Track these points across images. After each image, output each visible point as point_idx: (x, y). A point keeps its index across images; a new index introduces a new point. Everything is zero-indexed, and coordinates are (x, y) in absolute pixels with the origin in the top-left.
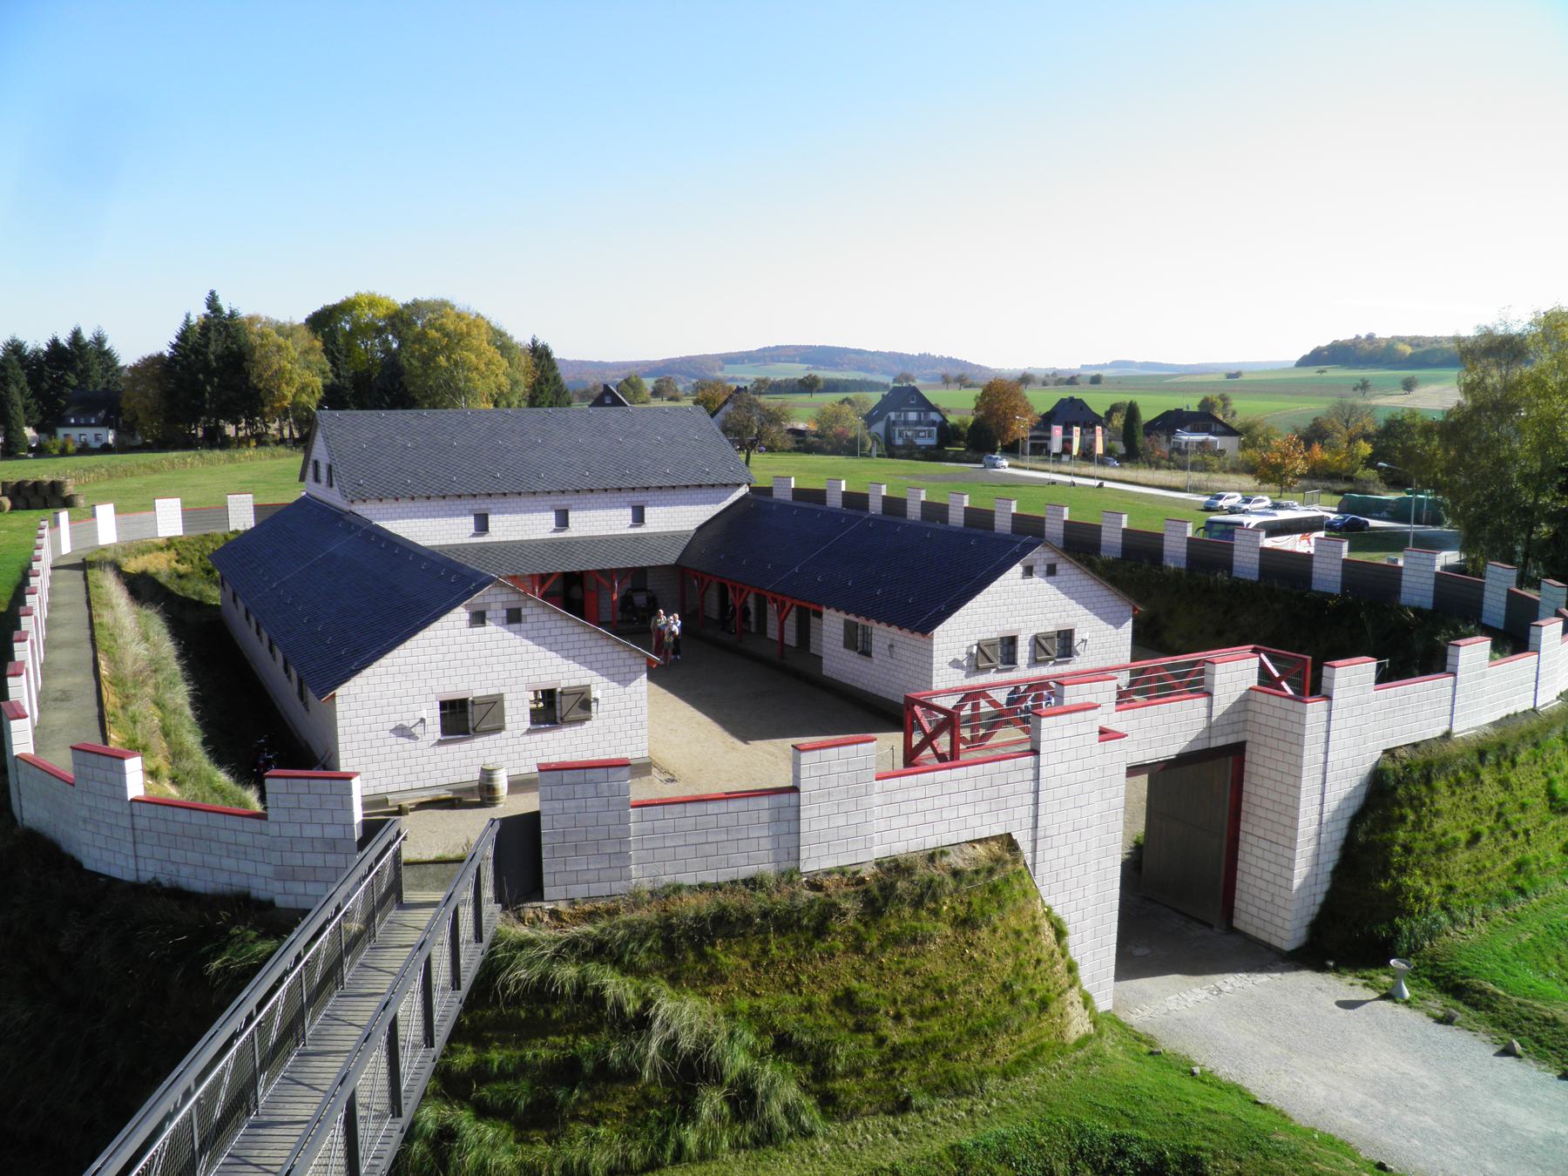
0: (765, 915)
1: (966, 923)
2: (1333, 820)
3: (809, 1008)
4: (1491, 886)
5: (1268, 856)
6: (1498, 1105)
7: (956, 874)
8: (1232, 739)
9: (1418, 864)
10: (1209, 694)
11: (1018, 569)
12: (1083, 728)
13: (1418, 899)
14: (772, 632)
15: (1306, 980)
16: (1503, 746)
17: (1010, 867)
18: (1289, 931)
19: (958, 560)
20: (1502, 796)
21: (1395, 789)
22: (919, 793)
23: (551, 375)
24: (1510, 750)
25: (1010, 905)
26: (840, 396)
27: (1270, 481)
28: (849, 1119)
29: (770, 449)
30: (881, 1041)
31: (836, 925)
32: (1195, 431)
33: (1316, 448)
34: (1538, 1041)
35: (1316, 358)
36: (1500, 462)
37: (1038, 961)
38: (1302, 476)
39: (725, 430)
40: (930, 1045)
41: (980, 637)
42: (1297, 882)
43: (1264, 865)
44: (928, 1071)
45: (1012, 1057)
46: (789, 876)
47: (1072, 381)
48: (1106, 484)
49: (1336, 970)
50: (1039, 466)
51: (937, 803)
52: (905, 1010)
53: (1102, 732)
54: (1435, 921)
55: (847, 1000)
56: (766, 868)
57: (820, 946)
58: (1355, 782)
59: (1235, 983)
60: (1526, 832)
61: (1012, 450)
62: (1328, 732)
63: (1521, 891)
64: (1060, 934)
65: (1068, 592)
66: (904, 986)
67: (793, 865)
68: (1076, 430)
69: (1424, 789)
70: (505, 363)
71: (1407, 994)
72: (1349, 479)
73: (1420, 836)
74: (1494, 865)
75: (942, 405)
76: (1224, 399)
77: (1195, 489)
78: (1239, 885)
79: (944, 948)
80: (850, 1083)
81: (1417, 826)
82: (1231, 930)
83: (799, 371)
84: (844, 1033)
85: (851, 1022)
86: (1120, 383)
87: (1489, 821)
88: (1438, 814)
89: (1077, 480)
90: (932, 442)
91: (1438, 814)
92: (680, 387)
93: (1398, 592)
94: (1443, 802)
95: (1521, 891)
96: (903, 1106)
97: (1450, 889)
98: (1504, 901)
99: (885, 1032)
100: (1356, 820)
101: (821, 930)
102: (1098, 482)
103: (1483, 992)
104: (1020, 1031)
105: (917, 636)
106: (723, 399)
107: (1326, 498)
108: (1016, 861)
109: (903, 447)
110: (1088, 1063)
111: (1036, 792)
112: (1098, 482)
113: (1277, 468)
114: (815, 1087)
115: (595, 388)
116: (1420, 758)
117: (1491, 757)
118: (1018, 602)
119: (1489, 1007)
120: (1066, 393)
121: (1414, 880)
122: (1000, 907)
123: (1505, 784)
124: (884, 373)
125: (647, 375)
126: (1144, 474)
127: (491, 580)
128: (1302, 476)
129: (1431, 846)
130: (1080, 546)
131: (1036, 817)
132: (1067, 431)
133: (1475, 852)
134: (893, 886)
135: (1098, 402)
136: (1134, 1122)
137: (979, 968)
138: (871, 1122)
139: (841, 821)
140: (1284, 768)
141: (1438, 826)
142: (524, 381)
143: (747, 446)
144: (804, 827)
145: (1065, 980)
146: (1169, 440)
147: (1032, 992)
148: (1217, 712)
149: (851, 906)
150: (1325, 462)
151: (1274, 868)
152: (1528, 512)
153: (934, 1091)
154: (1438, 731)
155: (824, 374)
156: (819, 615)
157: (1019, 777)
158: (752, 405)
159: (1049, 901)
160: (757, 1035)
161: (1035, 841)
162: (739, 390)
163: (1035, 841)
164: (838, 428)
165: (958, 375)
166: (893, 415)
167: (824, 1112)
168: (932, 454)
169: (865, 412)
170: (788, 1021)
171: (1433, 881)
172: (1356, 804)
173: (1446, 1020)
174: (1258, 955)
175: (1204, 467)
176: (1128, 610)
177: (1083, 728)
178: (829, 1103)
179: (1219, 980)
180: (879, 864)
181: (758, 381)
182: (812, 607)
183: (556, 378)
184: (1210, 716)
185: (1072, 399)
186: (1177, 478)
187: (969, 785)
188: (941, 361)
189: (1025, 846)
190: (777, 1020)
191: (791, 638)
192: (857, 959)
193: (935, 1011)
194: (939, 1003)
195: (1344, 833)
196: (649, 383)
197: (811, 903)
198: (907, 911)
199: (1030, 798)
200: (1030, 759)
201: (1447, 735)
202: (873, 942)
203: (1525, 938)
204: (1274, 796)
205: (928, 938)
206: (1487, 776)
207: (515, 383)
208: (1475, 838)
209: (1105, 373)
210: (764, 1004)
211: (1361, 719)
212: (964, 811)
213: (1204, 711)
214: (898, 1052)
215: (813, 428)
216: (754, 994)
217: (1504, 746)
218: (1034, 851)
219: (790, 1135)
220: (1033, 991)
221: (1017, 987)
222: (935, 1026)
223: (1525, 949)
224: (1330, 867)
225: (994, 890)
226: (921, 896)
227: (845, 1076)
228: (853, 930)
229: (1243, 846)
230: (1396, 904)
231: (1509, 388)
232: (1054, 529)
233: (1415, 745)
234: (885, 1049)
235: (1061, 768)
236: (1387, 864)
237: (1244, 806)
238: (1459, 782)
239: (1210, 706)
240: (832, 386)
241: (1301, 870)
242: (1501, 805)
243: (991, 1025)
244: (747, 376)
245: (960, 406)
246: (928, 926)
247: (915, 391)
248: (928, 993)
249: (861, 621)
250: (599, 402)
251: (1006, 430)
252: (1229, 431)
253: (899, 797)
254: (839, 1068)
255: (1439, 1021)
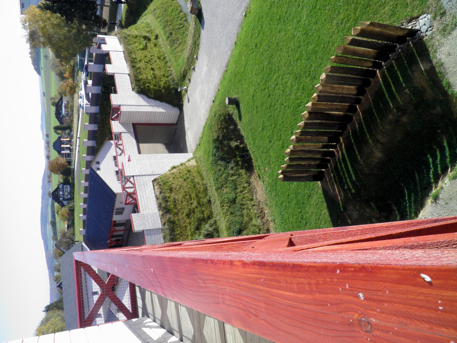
0: (171, 235)
1: (171, 190)
2: (149, 103)
3: (190, 223)
4: (163, 65)
5: (158, 117)
6: (203, 74)
7: (161, 193)
8: (132, 127)
9: (158, 83)
10: (121, 133)
11: (98, 172)
12: (128, 165)
13: (166, 83)
14: (122, 233)
15: (185, 108)
16: (131, 61)
17: (159, 180)
18: (175, 112)
19: (97, 186)
20: (143, 62)
21: (141, 88)
22: (143, 203)
23: (55, 304)
24: (132, 60)
25: (167, 180)
26: (56, 215)
27: (75, 90)
28: (212, 213)
29: (74, 235)
30: (196, 207)
31: (172, 219)
32: (61, 109)
33: (65, 75)
34: (192, 62)
35: (38, 69)
36: (65, 38)
37: (180, 173)
38: (74, 80)
39: (69, 249)
40: (197, 196)
41: (116, 180)
42: (164, 111)
43: (161, 118)
44: (202, 196)
45: (199, 178)
46: (162, 230)
47: (48, 143)
48: (78, 136)
49: (182, 102)
50: (74, 155)
51: (145, 198)
52: (190, 202)
53: (129, 161)
54: (171, 79)
55: (188, 215)
56: (161, 236)
57: (177, 222)
58: (140, 98)
59: (187, 125)
60: (151, 56)
61: (69, 163)
62: (128, 105)
63: (164, 58)
64: (174, 167)
65: (104, 158)
66: (185, 203)
67: (160, 230)
68: (62, 146)
69: (141, 81)
70: (52, 319)
71: (186, 87)
72: (74, 67)
73: (152, 82)
74: (159, 64)
75: (57, 183)
76: (51, 99)
77: (78, 111)
78: (166, 123)
79: (176, 194)
80: (205, 213)
81: (150, 83)
82: (177, 124)
83: (49, 227)
84: (195, 215)
85: (193, 214)
86: (48, 128)
87: (149, 65)
88: (147, 78)
89: (78, 145)
90: (68, 186)
91: (147, 78)
92: (57, 263)
93: (99, 73)
94: (144, 76)
95: (164, 58)
96: (209, 201)
97: (164, 75)
98: (166, 63)
99: (195, 207)
100: (149, 97)
101: (174, 222)
102: (78, 139)
103: (184, 71)
104: (194, 176)
105: (117, 197)
106: (59, 251)
107: (79, 75)
108: (158, 179)
109: (71, 195)
110: (200, 161)
111: (142, 175)
112: (78, 139)
113: (71, 88)
114: (206, 221)
115: (59, 290)
116: (134, 82)
117: (134, 64)
118: (107, 172)
119: (187, 71)
120: (52, 148)
121: (162, 84)
122: (168, 182)
123: (140, 61)
124: (48, 200)
125: (53, 274)
126: (75, 125)
127: (109, 309)
128: (74, 80)
129: (154, 80)
130: (93, 151)
131: (148, 175)
132: (63, 149)
133: (155, 69)
134: (163, 207)
135: (54, 137)
136: (209, 152)
137: (181, 187)
138: (213, 208)
139: (150, 220)
140: (137, 115)
141: (150, 78)
142: (57, 312)
143: (73, 242)
144: (152, 228)
145: (184, 166)
146: (65, 117)
147: (186, 174)
148: (125, 131)
149: (168, 216)
150: (69, 73)
151: (161, 116)
152: (78, 30)
153: (206, 195)
154: (128, 77)
155: (50, 219)
156: (115, 221)
157: (139, 180)
158: (61, 242)
159: (167, 171)
160: (196, 234)
161: (154, 175)
162: (56, 246)
163: (154, 175)
164: (66, 215)
165: (47, 179)
166: (61, 199)
167: (211, 218)
168: (72, 186)
169: (61, 207)
170: (193, 227)
171: (162, 79)
172: (145, 97)
173: (190, 80)
174: (181, 118)
175: (72, 107)
176: (107, 141)
177: (128, 165)
178: (209, 218)
179: (186, 128)
180: (159, 210)
181: (53, 240)
182: (113, 223)
183: (56, 303)
184: (126, 132)
185: (53, 146)
186: (75, 116)
187: (141, 191)
188: (43, 183)
189: (155, 177)
190: (193, 230)
191: (122, 228)
192: (180, 214)
193: (190, 196)
194: (188, 195)
195: (152, 100)
196: (56, 274)
197: (168, 225)
198: (169, 204)
199: (144, 177)
200: (135, 178)
201: (129, 75)
202: (175, 211)
203: (174, 59)
204: (144, 117)
205: (175, 199)
206: (138, 66)
207: (58, 315)
208: (152, 69)
209: (45, 133)
210: (190, 234)
211: (126, 98)
212: (147, 192)
213: (125, 134)
214: (199, 203)
215: (66, 222)
216: (188, 236)
217: (132, 62)
218: (156, 175)
219: (216, 225)
220: (185, 173)
221: (185, 177)
222: (193, 195)
223: (176, 60)
224: (160, 103)
225: (164, 184)
226: (165, 201)
227: (204, 214)
228: (173, 215)
229: (157, 122)
230: (167, 88)
231: (44, 36)
232: (89, 158)
233: (131, 83)
234: (198, 206)
235: (137, 170)
236: (158, 90)
237: (147, 123)
238: (140, 72)
239: (124, 133)
240: (53, 216)
241: (161, 110)
242: (145, 62)
243: (193, 183)
244: (52, 243)
245: (57, 179)
246: (172, 199)
247: (53, 193)
248: (186, 197)
249: (115, 211)
250: (61, 288)
251: (64, 165)
252: (61, 99)
253: (144, 207)
254: (202, 216)
255: (190, 82)
